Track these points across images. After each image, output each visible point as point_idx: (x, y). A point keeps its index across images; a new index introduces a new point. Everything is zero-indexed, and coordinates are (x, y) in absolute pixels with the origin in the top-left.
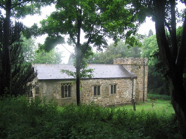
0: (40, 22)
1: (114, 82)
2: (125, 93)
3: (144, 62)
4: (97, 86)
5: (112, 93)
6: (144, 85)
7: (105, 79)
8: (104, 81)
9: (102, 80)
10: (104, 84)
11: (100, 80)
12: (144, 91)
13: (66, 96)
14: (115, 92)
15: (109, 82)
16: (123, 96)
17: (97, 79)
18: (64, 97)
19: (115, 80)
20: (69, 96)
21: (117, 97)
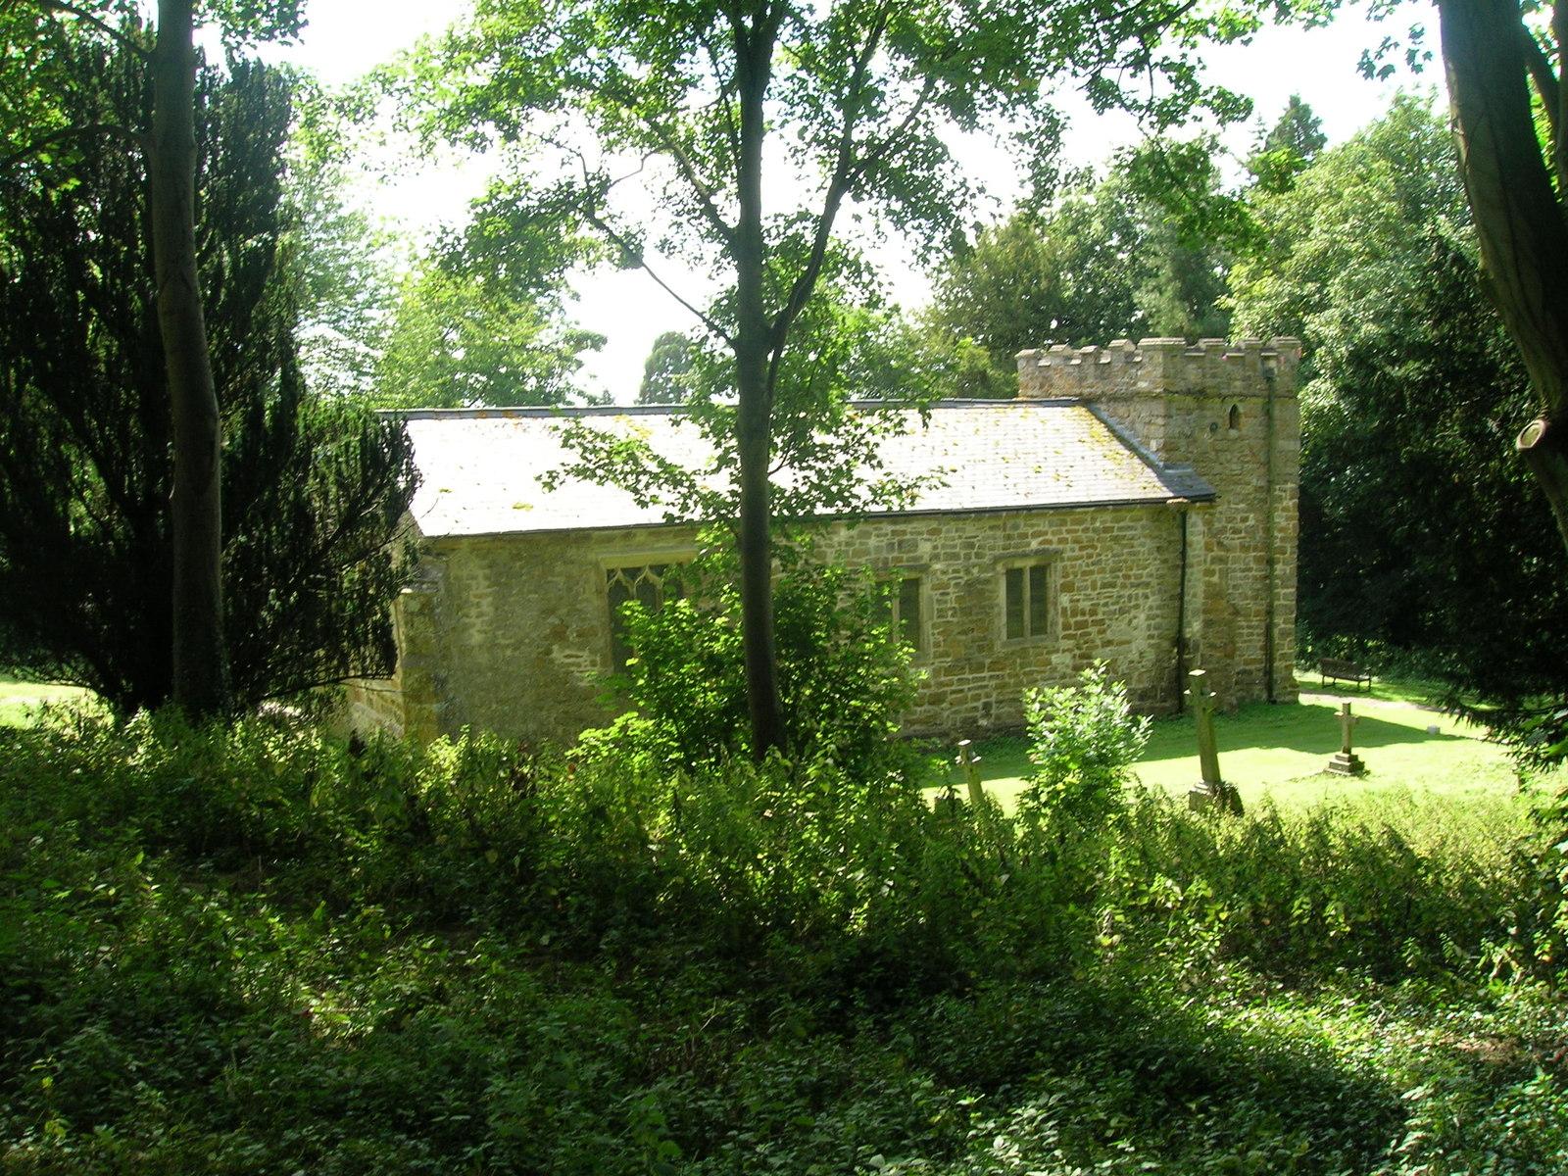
9: (934, 525)
14: (1040, 625)
19: (1043, 525)
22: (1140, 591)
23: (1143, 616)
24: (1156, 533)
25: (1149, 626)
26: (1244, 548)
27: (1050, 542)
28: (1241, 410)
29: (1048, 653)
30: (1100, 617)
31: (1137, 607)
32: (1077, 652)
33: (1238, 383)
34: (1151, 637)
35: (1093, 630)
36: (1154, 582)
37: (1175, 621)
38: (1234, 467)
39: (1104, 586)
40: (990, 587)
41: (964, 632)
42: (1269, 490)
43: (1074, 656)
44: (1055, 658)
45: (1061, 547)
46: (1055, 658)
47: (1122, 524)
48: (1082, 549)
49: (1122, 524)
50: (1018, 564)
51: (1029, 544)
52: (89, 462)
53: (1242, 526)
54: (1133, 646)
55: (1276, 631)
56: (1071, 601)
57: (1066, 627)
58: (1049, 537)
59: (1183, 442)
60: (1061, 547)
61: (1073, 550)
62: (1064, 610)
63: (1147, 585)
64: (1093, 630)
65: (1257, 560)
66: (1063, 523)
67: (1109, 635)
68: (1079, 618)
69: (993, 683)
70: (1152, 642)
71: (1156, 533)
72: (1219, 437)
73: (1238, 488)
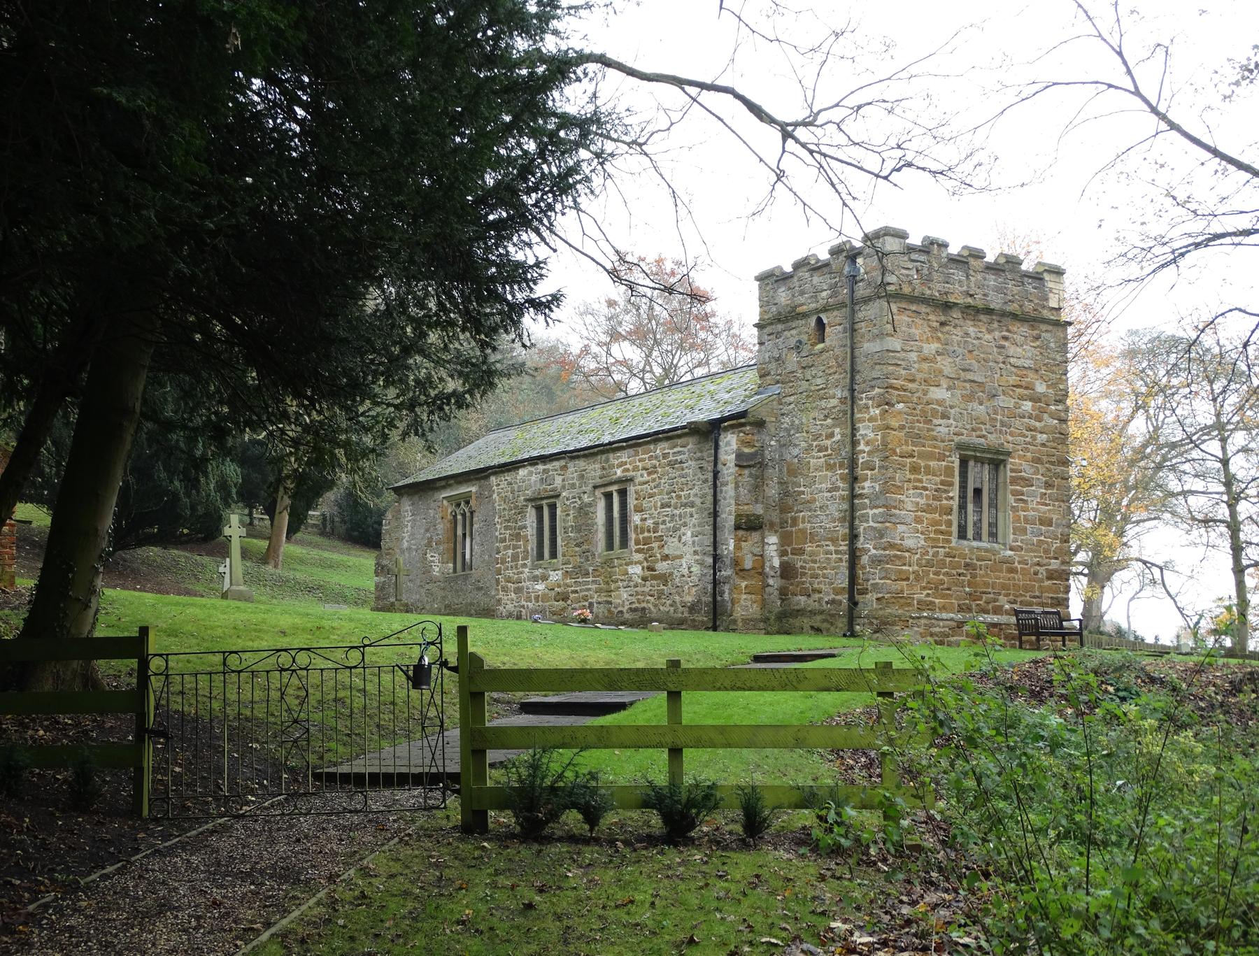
0: (770, 280)
1: (619, 472)
2: (672, 546)
3: (853, 279)
4: (544, 502)
5: (610, 546)
6: (854, 479)
7: (574, 455)
8: (574, 467)
9: (562, 463)
10: (573, 486)
11: (557, 464)
12: (853, 537)
13: (978, 537)
14: (624, 543)
15: (593, 469)
16: (662, 567)
17: (544, 463)
18: (980, 540)
19: (624, 456)
20: (993, 535)
21: (636, 570)
22: (688, 510)
23: (689, 534)
24: (699, 455)
25: (694, 542)
26: (830, 467)
27: (628, 470)
28: (825, 321)
29: (627, 564)
30: (660, 534)
31: (685, 525)
32: (645, 564)
33: (824, 294)
34: (696, 553)
35: (655, 545)
36: (698, 501)
37: (718, 534)
38: (819, 381)
39: (663, 506)
40: (592, 509)
41: (577, 545)
42: (853, 400)
43: (643, 568)
44: (631, 570)
45: (634, 474)
46: (631, 570)
47: (675, 450)
48: (649, 474)
49: (675, 450)
50: (609, 489)
51: (616, 473)
52: (229, 445)
53: (828, 442)
54: (684, 561)
55: (865, 560)
56: (642, 520)
57: (637, 543)
58: (628, 466)
59: (773, 366)
60: (634, 474)
61: (642, 476)
62: (636, 527)
63: (692, 505)
64: (655, 545)
65: (842, 478)
66: (637, 454)
67: (666, 551)
68: (646, 534)
69: (594, 587)
70: (697, 557)
71: (699, 455)
72: (804, 354)
73: (823, 404)
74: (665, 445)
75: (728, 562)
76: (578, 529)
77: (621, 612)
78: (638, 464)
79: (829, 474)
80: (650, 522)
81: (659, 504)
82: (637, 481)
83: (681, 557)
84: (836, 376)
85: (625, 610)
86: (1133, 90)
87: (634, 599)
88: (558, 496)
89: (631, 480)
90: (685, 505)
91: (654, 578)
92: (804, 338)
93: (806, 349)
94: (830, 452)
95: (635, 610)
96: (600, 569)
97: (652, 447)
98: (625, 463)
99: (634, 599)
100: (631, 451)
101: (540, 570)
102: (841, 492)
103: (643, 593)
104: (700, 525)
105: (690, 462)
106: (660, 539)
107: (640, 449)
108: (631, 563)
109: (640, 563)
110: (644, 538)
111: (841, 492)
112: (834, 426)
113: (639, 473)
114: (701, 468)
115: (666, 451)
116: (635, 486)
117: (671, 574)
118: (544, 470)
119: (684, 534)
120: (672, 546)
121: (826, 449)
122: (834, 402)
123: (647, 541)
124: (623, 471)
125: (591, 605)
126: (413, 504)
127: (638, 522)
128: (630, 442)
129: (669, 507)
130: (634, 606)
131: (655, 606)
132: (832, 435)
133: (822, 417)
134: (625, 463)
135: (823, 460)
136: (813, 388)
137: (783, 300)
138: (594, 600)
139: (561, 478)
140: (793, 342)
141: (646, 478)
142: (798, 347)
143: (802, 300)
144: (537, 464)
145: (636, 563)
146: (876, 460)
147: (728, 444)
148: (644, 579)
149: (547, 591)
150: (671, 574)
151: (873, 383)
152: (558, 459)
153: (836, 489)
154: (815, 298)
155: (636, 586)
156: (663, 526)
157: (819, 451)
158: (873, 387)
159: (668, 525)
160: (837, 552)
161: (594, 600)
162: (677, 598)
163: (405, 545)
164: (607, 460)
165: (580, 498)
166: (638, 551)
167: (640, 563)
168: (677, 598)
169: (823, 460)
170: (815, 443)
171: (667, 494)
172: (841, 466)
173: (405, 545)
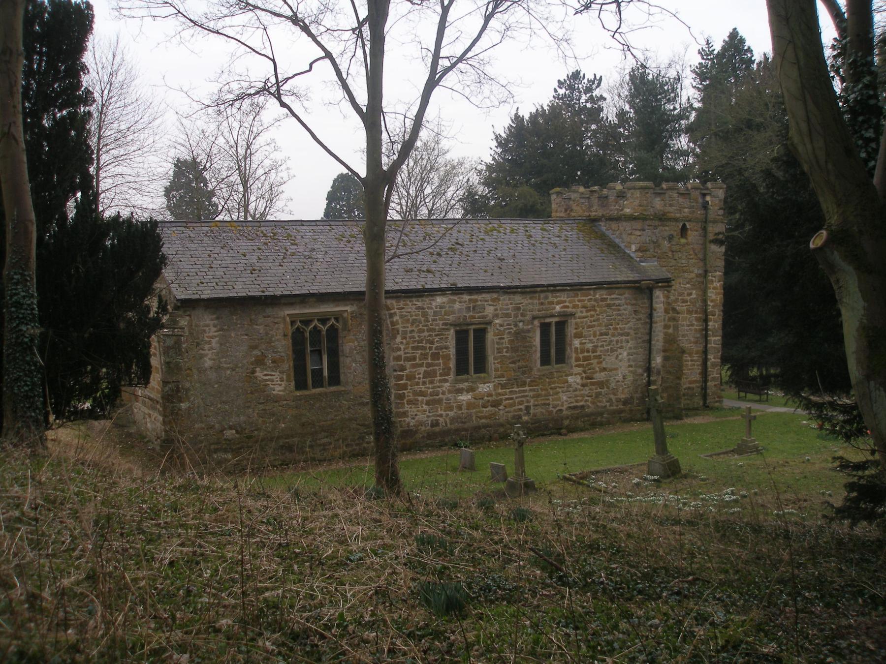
8: (505, 300)
9: (495, 296)
14: (561, 358)
16: (600, 376)
19: (563, 297)
22: (624, 338)
23: (625, 354)
24: (634, 302)
25: (629, 360)
26: (690, 312)
27: (567, 307)
28: (688, 227)
29: (567, 375)
30: (598, 353)
31: (621, 347)
32: (584, 375)
34: (630, 366)
35: (594, 361)
38: (683, 261)
39: (601, 334)
40: (530, 335)
41: (513, 362)
43: (582, 378)
46: (570, 379)
47: (613, 296)
48: (587, 311)
49: (613, 296)
53: (688, 298)
56: (581, 344)
57: (577, 359)
58: (567, 304)
60: (574, 310)
61: (581, 312)
62: (576, 349)
63: (628, 334)
65: (697, 319)
66: (577, 295)
67: (604, 365)
68: (586, 354)
69: (531, 394)
70: (631, 369)
71: (634, 302)
73: (686, 275)
74: (604, 292)
75: (655, 371)
76: (514, 350)
77: (561, 410)
78: (577, 303)
79: (689, 316)
80: (590, 346)
81: (598, 333)
82: (577, 315)
83: (616, 369)
84: (694, 261)
85: (564, 408)
86: (361, 20)
87: (572, 400)
88: (489, 323)
89: (572, 315)
90: (622, 335)
91: (593, 384)
92: (675, 234)
93: (676, 240)
94: (689, 304)
95: (575, 408)
96: (537, 380)
97: (592, 292)
98: (565, 302)
99: (572, 400)
100: (571, 293)
101: (466, 384)
102: (695, 327)
103: (582, 396)
104: (635, 348)
105: (626, 306)
106: (599, 357)
107: (579, 293)
108: (571, 374)
109: (579, 374)
110: (583, 357)
111: (695, 327)
112: (693, 289)
113: (579, 310)
114: (635, 311)
115: (605, 296)
116: (575, 318)
117: (607, 381)
118: (470, 300)
119: (620, 354)
120: (609, 361)
121: (687, 302)
122: (693, 275)
123: (586, 359)
124: (562, 308)
125: (528, 408)
126: (218, 318)
127: (578, 346)
128: (575, 287)
129: (607, 335)
130: (572, 405)
131: (593, 403)
132: (691, 294)
133: (685, 283)
134: (565, 302)
135: (685, 308)
136: (679, 265)
137: (658, 206)
138: (531, 404)
139: (492, 308)
140: (666, 234)
141: (584, 314)
142: (671, 238)
143: (671, 209)
144: (462, 294)
145: (576, 374)
146: (717, 311)
147: (658, 297)
148: (583, 385)
149: (473, 400)
150: (607, 381)
151: (717, 268)
152: (489, 292)
153: (692, 325)
154: (680, 211)
155: (575, 390)
156: (602, 349)
157: (683, 302)
158: (716, 271)
159: (606, 348)
160: (692, 361)
161: (531, 404)
162: (612, 396)
163: (208, 363)
164: (546, 298)
165: (516, 325)
166: (577, 366)
167: (579, 374)
168: (612, 396)
169: (685, 308)
170: (680, 298)
171: (605, 326)
172: (696, 312)
173: (208, 363)
